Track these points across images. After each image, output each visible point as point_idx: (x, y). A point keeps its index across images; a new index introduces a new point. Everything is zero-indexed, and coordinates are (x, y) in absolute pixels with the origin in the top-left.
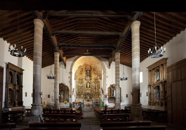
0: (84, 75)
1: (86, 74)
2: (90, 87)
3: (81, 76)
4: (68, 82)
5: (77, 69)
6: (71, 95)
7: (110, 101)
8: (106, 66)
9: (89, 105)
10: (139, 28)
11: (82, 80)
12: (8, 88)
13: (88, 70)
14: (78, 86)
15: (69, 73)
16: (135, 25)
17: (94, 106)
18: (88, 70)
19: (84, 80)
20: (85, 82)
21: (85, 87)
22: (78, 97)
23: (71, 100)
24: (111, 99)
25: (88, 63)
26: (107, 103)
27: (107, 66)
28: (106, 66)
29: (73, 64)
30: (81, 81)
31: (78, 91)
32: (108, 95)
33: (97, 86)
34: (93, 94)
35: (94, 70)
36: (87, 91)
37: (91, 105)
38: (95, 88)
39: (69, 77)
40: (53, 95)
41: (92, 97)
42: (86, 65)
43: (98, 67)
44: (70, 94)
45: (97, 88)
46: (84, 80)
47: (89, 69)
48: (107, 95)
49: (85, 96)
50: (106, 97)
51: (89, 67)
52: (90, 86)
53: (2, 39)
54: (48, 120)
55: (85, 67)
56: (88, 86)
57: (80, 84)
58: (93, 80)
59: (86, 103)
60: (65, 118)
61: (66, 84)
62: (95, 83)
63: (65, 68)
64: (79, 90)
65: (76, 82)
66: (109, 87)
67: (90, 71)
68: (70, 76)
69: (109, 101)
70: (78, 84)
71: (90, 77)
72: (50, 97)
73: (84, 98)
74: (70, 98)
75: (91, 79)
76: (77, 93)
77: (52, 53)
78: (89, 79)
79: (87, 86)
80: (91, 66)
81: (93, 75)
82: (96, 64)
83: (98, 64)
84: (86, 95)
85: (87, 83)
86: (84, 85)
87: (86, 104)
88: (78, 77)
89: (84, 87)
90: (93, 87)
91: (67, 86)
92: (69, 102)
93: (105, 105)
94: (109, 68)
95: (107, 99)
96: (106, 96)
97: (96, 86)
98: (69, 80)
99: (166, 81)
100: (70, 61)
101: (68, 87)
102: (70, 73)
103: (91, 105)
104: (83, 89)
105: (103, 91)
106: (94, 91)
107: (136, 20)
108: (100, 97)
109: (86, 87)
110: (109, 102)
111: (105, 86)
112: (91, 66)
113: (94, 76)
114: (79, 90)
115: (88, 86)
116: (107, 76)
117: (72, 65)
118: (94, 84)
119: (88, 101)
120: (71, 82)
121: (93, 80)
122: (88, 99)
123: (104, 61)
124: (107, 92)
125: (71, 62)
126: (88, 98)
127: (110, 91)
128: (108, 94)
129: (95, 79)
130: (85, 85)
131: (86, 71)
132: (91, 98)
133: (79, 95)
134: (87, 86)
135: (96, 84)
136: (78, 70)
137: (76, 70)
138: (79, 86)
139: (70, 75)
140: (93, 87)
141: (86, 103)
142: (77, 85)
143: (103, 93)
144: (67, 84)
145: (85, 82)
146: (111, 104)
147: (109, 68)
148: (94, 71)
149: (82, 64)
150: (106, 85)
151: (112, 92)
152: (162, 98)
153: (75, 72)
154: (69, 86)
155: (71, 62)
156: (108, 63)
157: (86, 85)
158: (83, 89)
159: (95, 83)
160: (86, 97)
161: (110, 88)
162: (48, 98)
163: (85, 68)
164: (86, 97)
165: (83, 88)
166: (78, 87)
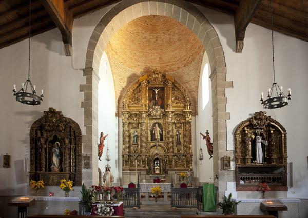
0: (145, 100)
1: (150, 100)
2: (161, 139)
3: (135, 108)
4: (80, 105)
5: (124, 84)
6: (89, 158)
7: (242, 182)
8: (223, 41)
9: (159, 196)
11: (138, 115)
13: (155, 88)
14: (127, 134)
17: (176, 196)
18: (155, 88)
19: (144, 116)
20: (148, 123)
21: (147, 138)
22: (128, 167)
23: (90, 176)
24: (245, 175)
25: (156, 66)
27: (229, 44)
28: (223, 41)
30: (134, 121)
31: (127, 150)
32: (236, 160)
33: (185, 136)
34: (171, 161)
35: (174, 87)
36: (154, 151)
37: (166, 196)
38: (178, 142)
39: (82, 88)
40: (22, 158)
41: (168, 168)
42: (148, 72)
43: (186, 78)
44: (84, 153)
45: (182, 140)
46: (144, 116)
47: (159, 82)
48: (232, 157)
49: (149, 164)
50: (228, 165)
51: (160, 76)
52: (161, 135)
55: (146, 76)
56: (158, 136)
57: (132, 131)
58: (171, 118)
59: (147, 187)
60: (137, 193)
62: (178, 125)
63: (68, 54)
64: (129, 147)
66: (239, 127)
67: (162, 89)
69: (238, 185)
70: (126, 128)
71: (162, 107)
72: (12, 164)
73: (144, 173)
74: (84, 171)
75: (165, 115)
76: (123, 157)
78: (159, 112)
79: (153, 135)
80: (164, 76)
82: (178, 68)
83: (185, 66)
84: (151, 161)
86: (143, 133)
87: (150, 190)
88: (127, 109)
89: (144, 139)
90: (171, 139)
91: (74, 122)
93: (221, 200)
94: (238, 49)
95: (232, 175)
96: (226, 164)
97: (181, 136)
100: (100, 55)
101: (77, 126)
102: (84, 70)
103: (166, 196)
104: (141, 146)
105: (210, 145)
106: (176, 151)
108: (192, 170)
109: (149, 139)
110: (239, 188)
111: (221, 122)
112: (164, 76)
113: (173, 106)
114: (129, 147)
115: (158, 136)
116: (228, 79)
117: (95, 38)
118: (175, 130)
119: (157, 181)
120: (88, 105)
121: (171, 118)
122: (157, 174)
123: (217, 22)
124: (230, 146)
125: (90, 30)
126: (157, 172)
127: (243, 142)
128: (235, 152)
129: (177, 115)
130: (147, 133)
131: (151, 90)
132: (165, 172)
133: (127, 160)
134: (153, 135)
135: (181, 131)
137: (121, 89)
138: (129, 137)
139: (84, 80)
140: (171, 139)
141: (147, 187)
142: (124, 133)
143: (211, 152)
144: (72, 112)
145: (148, 123)
146: (248, 197)
147: (238, 49)
148: (173, 89)
149: (138, 71)
150: (228, 116)
151: (250, 147)
152: (29, 171)
153: (118, 97)
154: (81, 122)
155: (90, 30)
156: (231, 28)
157: (152, 132)
158: (141, 146)
159: (178, 125)
160: (150, 169)
161: (243, 133)
162: (4, 170)
163: (149, 82)
164: (150, 169)
165: (142, 141)
166: (127, 140)
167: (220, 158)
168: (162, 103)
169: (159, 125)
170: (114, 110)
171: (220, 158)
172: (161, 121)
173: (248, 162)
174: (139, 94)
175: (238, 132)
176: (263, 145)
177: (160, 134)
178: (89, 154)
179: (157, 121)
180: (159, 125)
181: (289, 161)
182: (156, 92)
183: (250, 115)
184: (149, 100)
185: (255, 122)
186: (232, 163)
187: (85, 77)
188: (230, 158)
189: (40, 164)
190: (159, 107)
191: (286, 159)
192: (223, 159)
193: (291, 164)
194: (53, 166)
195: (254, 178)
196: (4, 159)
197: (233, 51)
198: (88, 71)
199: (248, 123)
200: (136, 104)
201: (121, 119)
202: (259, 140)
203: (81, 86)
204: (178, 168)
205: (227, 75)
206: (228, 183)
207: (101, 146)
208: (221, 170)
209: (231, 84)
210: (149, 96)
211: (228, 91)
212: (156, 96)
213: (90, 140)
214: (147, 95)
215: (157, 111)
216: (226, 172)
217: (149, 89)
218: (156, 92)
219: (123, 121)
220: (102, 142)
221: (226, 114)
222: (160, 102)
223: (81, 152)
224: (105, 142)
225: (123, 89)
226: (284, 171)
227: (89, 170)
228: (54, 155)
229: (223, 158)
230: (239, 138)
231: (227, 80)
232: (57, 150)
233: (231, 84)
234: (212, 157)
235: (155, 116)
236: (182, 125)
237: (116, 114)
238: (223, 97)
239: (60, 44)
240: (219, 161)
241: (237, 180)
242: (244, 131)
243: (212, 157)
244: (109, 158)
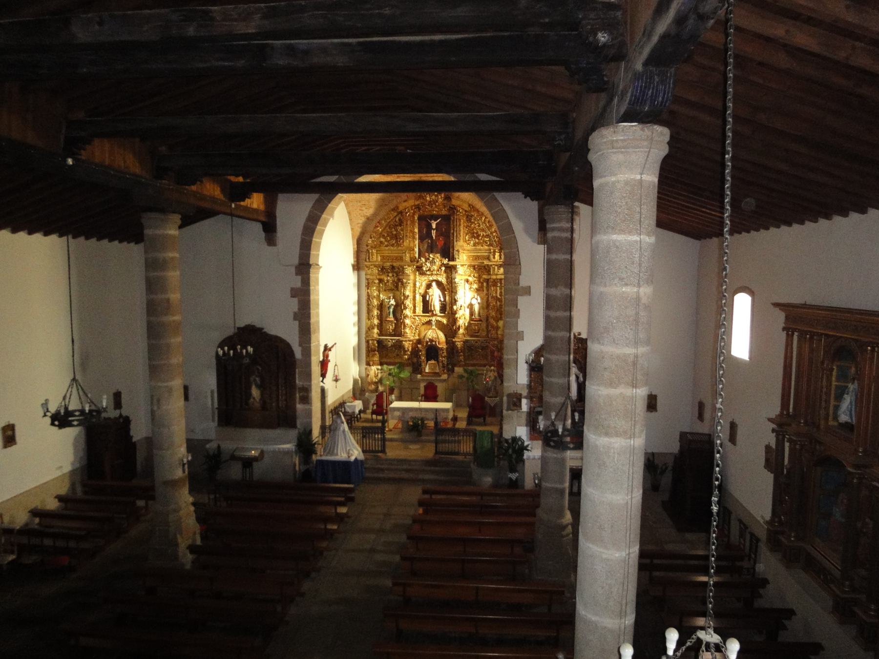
1: (421, 239)
4: (292, 315)
8: (518, 226)
10: (651, 178)
15: (293, 270)
16: (617, 158)
27: (527, 231)
29: (319, 218)
32: (530, 398)
48: (525, 392)
61: (274, 330)
65: (364, 283)
68: (297, 282)
74: (299, 406)
85: (429, 286)
92: (298, 422)
98: (294, 305)
101: (288, 346)
107: (628, 117)
115: (437, 306)
136: (375, 215)
139: (297, 282)
148: (469, 218)
153: (358, 233)
154: (293, 339)
157: (424, 297)
162: (187, 383)
166: (376, 312)
168: (445, 244)
169: (439, 284)
170: (351, 259)
174: (399, 228)
178: (306, 384)
179: (435, 278)
182: (434, 226)
184: (419, 238)
186: (524, 402)
187: (299, 278)
190: (438, 255)
192: (509, 395)
194: (252, 400)
198: (304, 267)
200: (393, 245)
201: (363, 273)
203: (292, 289)
204: (475, 362)
206: (518, 428)
207: (324, 364)
210: (419, 231)
212: (434, 233)
213: (308, 364)
214: (416, 230)
215: (433, 263)
217: (419, 219)
218: (434, 226)
219: (368, 277)
220: (326, 357)
221: (519, 333)
222: (441, 243)
223: (295, 382)
224: (332, 355)
225: (368, 219)
227: (307, 407)
228: (254, 387)
232: (257, 379)
236: (485, 284)
237: (353, 266)
244: (340, 377)
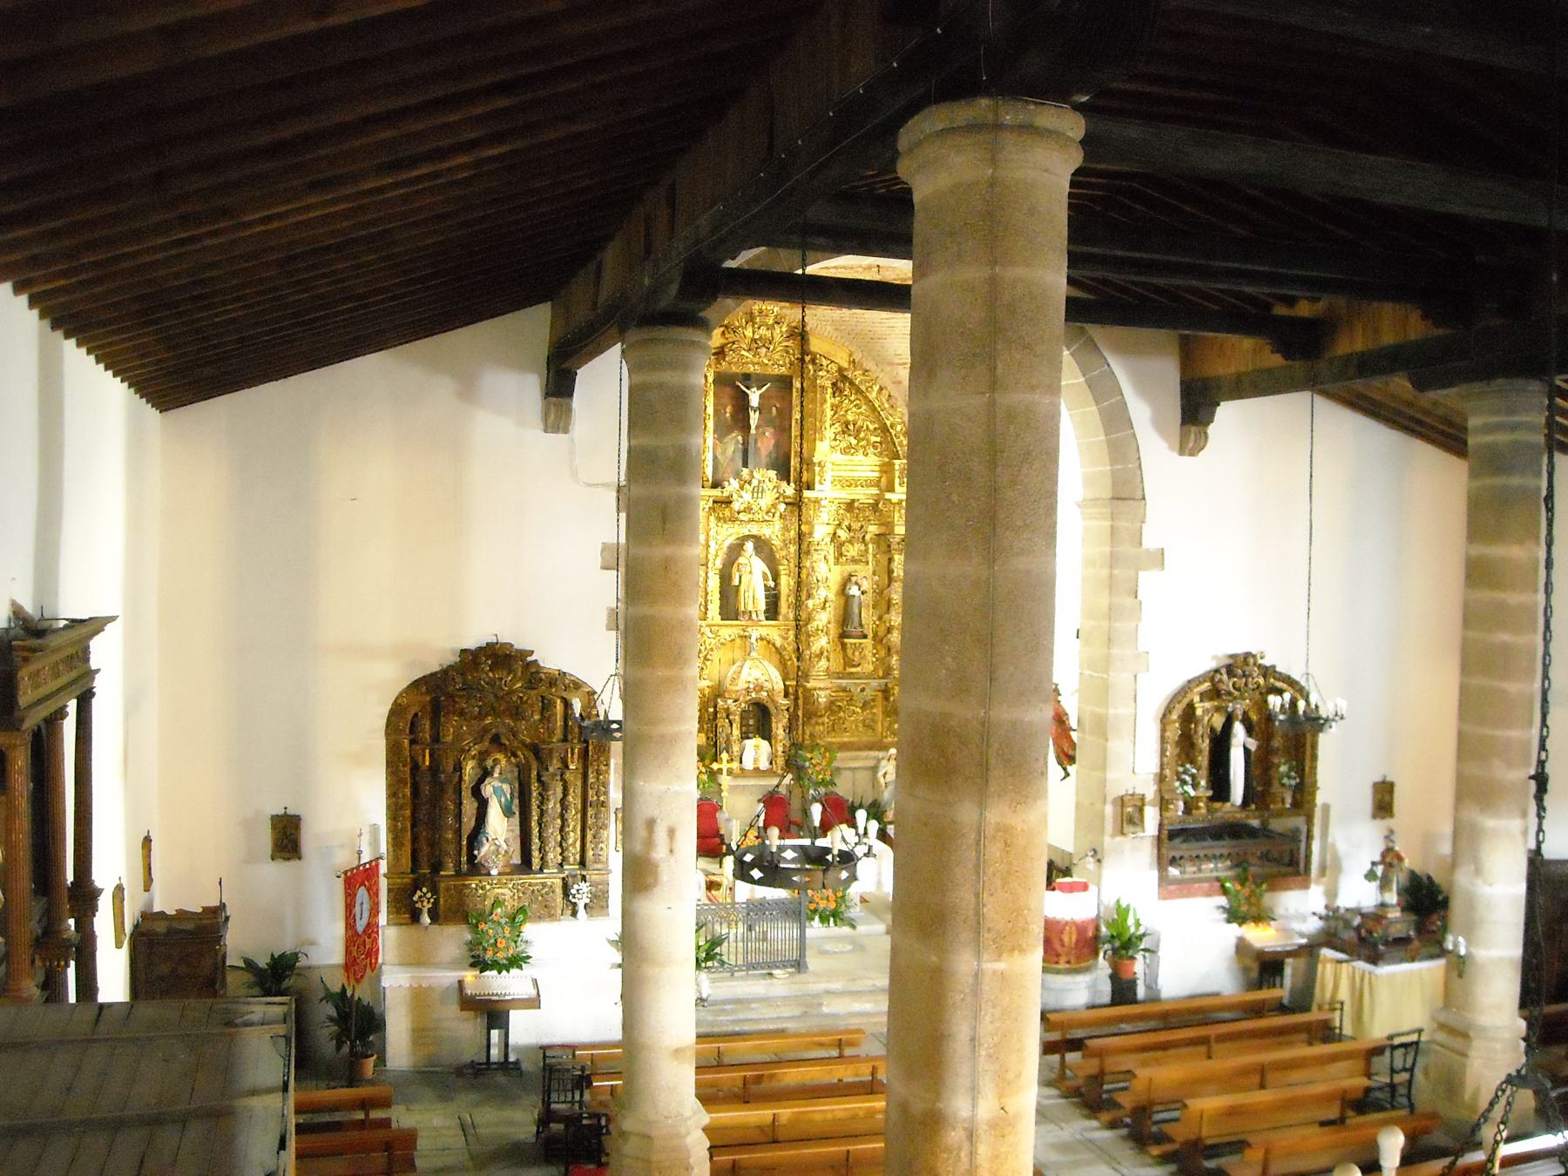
2: (772, 611)
4: (603, 619)
7: (1174, 872)
8: (1140, 411)
12: (1402, 941)
18: (747, 377)
26: (503, 762)
27: (1159, 425)
28: (1140, 411)
32: (1163, 804)
48: (1150, 791)
53: (7, 287)
54: (87, 985)
69: (1163, 880)
77: (851, 676)
78: (768, 498)
81: (824, 450)
99: (215, 994)
116: (1150, 541)
156: (1167, 371)
157: (725, 577)
161: (1189, 715)
162: (277, 872)
167: (1109, 799)
169: (763, 547)
171: (1109, 799)
172: (773, 531)
173: (1198, 808)
175: (1174, 716)
176: (1247, 751)
177: (767, 588)
179: (755, 530)
180: (763, 547)
181: (1320, 799)
183: (1215, 657)
185: (1227, 683)
188: (1142, 798)
189: (433, 844)
191: (1313, 794)
192: (1121, 802)
193: (1326, 808)
195: (1215, 857)
196: (274, 827)
197: (1171, 448)
199: (1206, 686)
202: (1239, 729)
205: (1147, 529)
208: (1113, 836)
209: (1158, 560)
211: (1148, 580)
212: (754, 418)
216: (1126, 842)
226: (1304, 829)
229: (1122, 798)
230: (1174, 732)
231: (1144, 546)
233: (1158, 560)
234: (1067, 775)
235: (748, 510)
238: (1129, 601)
239: (530, 387)
240: (1109, 810)
241: (1164, 861)
242: (1191, 707)
243: (1067, 775)
